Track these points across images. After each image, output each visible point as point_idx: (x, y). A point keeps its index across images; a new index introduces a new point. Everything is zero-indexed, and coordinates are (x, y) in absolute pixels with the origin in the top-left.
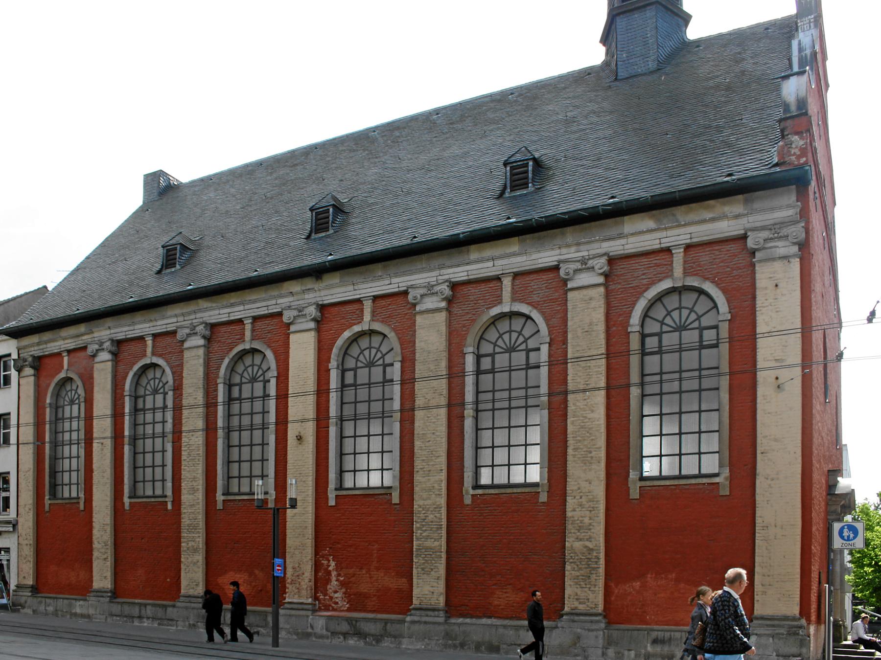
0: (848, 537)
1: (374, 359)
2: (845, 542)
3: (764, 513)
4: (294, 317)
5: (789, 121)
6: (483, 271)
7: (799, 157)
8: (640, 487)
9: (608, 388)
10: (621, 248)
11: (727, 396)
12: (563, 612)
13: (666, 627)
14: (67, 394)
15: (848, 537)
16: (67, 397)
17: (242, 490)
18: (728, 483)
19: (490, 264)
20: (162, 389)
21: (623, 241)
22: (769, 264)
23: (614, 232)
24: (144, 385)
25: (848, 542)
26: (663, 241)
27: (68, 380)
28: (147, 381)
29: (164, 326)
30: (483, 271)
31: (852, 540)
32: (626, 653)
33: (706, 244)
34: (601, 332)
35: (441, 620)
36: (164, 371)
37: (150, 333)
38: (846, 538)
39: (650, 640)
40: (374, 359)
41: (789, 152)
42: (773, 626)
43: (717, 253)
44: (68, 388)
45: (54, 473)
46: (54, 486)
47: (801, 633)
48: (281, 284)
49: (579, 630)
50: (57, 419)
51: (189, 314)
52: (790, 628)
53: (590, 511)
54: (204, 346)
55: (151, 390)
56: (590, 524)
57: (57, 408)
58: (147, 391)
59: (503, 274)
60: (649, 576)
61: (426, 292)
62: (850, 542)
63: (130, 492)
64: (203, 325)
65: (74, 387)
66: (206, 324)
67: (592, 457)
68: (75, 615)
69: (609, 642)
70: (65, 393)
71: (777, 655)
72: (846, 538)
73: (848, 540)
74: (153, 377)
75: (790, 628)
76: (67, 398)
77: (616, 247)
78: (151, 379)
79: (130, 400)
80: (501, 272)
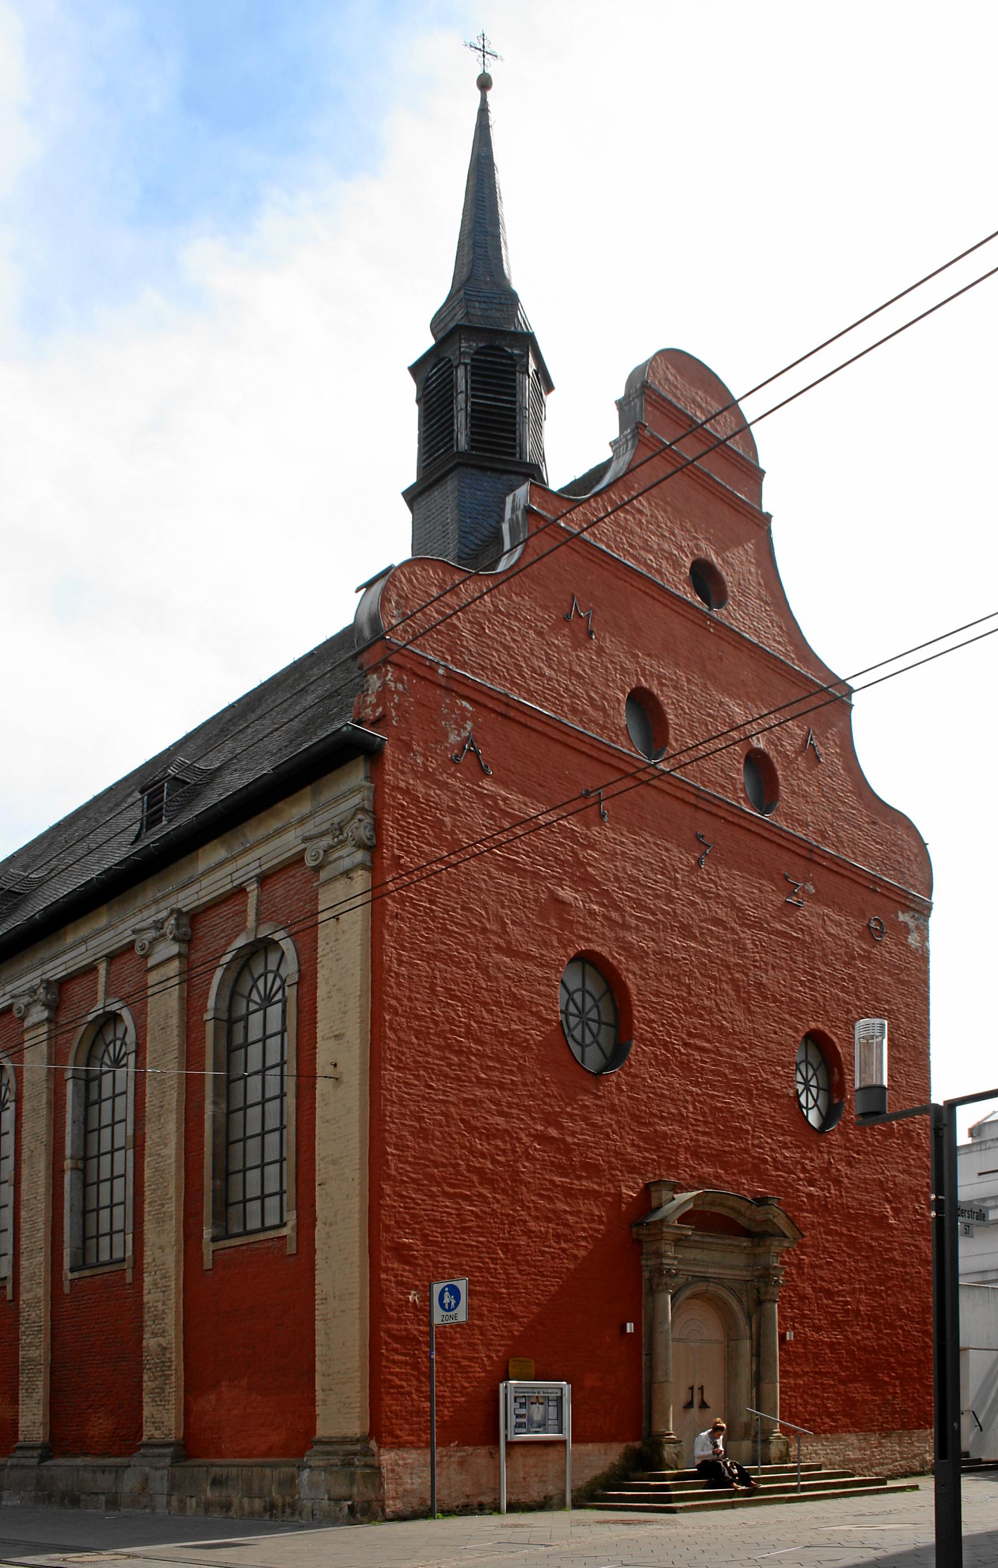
0: (450, 1304)
1: (272, 987)
2: (445, 1313)
3: (323, 1279)
4: (325, 851)
5: (365, 654)
6: (78, 960)
7: (375, 707)
8: (213, 1251)
9: (298, 1076)
10: (195, 897)
11: (294, 1101)
12: (139, 1443)
13: (119, 1460)
14: (254, 985)
15: (450, 1304)
16: (106, 1055)
17: (249, 1227)
18: (295, 1234)
19: (82, 949)
20: (280, 992)
21: (196, 887)
22: (331, 887)
23: (184, 877)
24: (100, 1056)
25: (449, 1314)
26: (236, 876)
27: (264, 946)
28: (251, 983)
29: (63, 967)
30: (78, 960)
31: (453, 1309)
32: (188, 1499)
33: (281, 870)
34: (175, 1027)
35: (34, 1462)
36: (283, 953)
37: (99, 955)
38: (447, 1307)
39: (209, 1481)
40: (272, 987)
41: (365, 701)
42: (328, 1453)
43: (292, 880)
44: (110, 1037)
45: (224, 1173)
46: (223, 1204)
47: (357, 1463)
48: (193, 854)
49: (147, 1469)
50: (231, 1050)
51: (165, 897)
52: (345, 1455)
53: (164, 1292)
54: (48, 1020)
55: (259, 1001)
56: (163, 1311)
57: (231, 1022)
58: (251, 1004)
59: (96, 960)
60: (224, 1383)
61: (331, 842)
62: (451, 1313)
63: (73, 1255)
64: (175, 916)
65: (120, 1034)
66: (179, 911)
67: (164, 1213)
68: (103, 1493)
69: (174, 1486)
70: (104, 1047)
71: (329, 1499)
72: (447, 1307)
73: (450, 1310)
74: (262, 970)
75: (345, 1455)
76: (255, 996)
77: (188, 899)
78: (260, 977)
79: (75, 1085)
80: (93, 959)
